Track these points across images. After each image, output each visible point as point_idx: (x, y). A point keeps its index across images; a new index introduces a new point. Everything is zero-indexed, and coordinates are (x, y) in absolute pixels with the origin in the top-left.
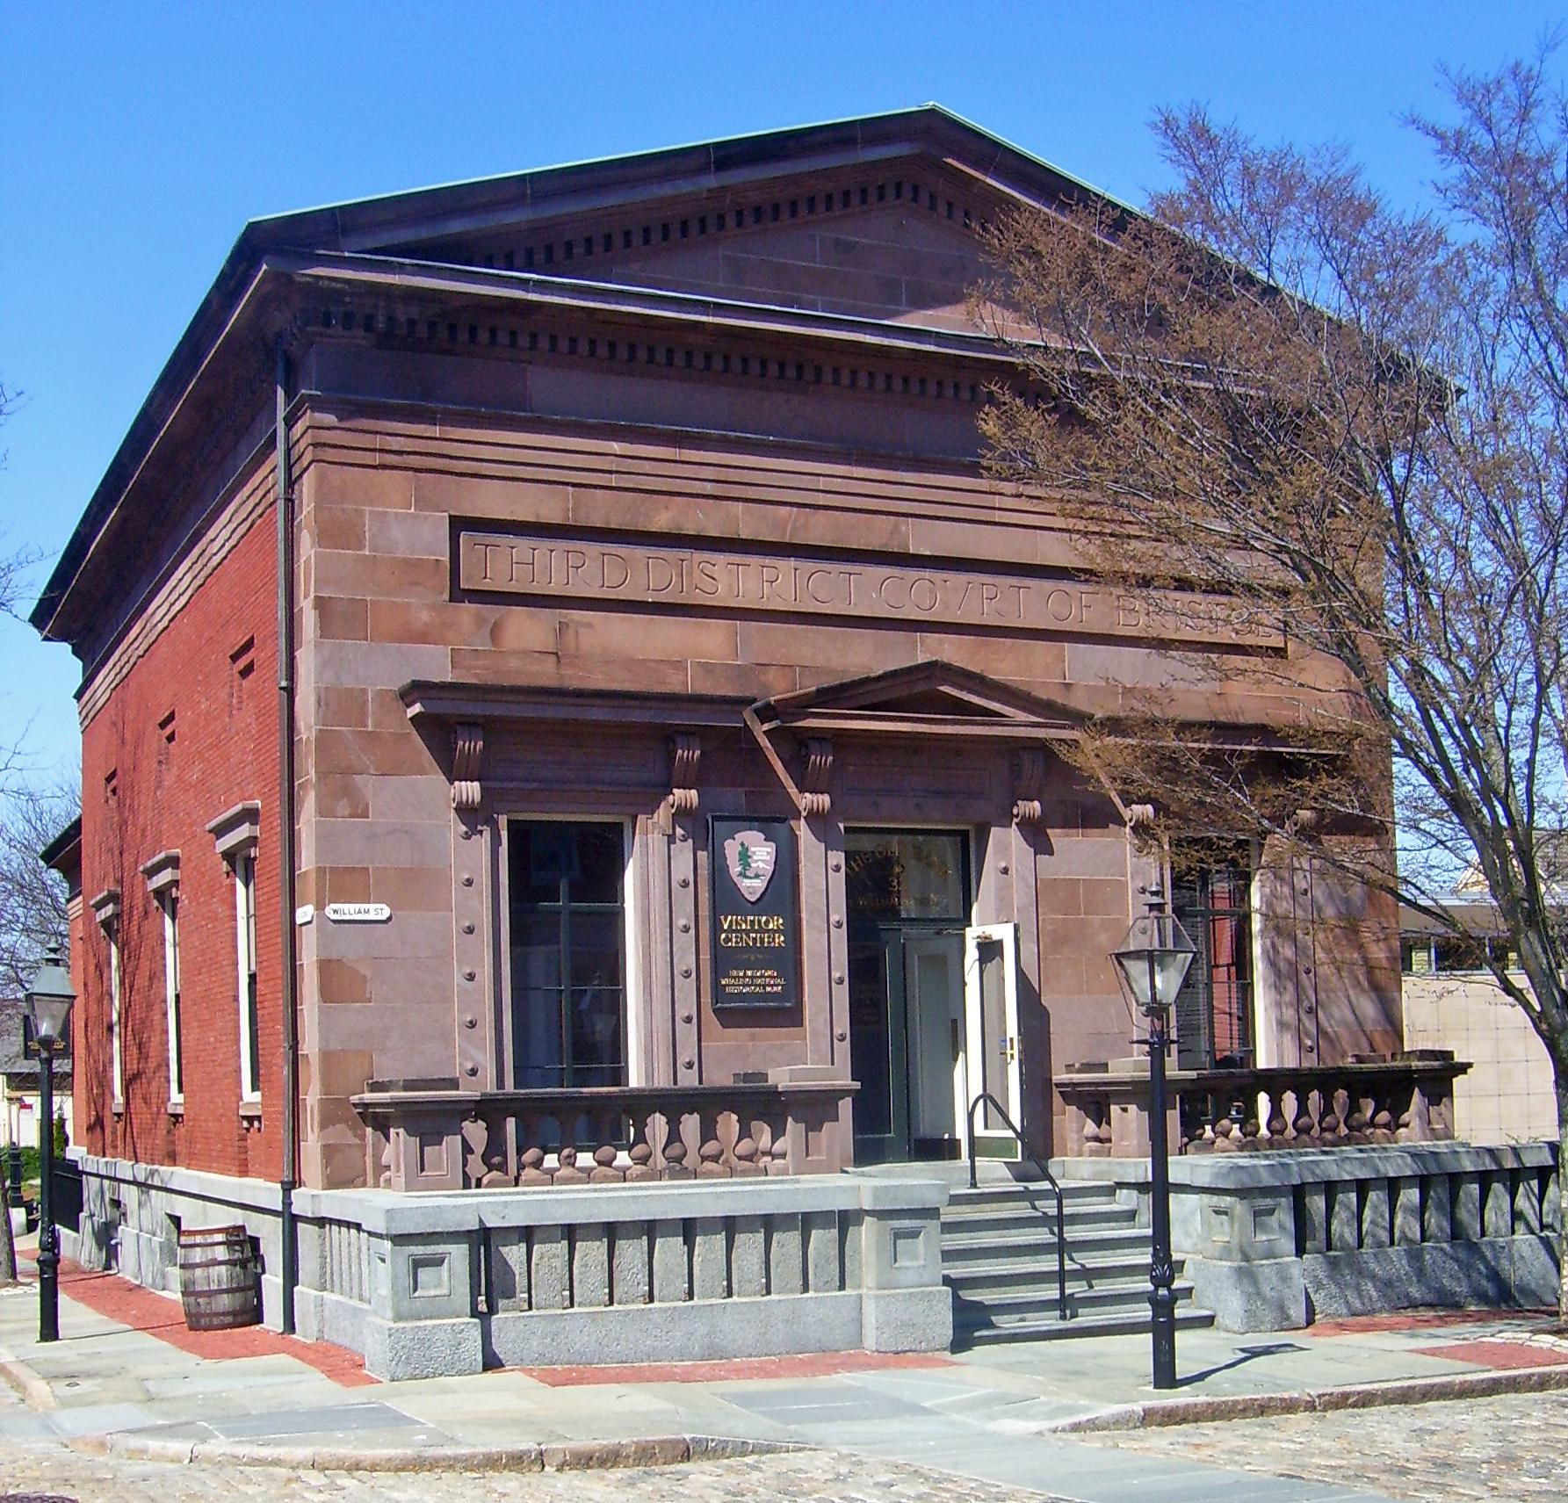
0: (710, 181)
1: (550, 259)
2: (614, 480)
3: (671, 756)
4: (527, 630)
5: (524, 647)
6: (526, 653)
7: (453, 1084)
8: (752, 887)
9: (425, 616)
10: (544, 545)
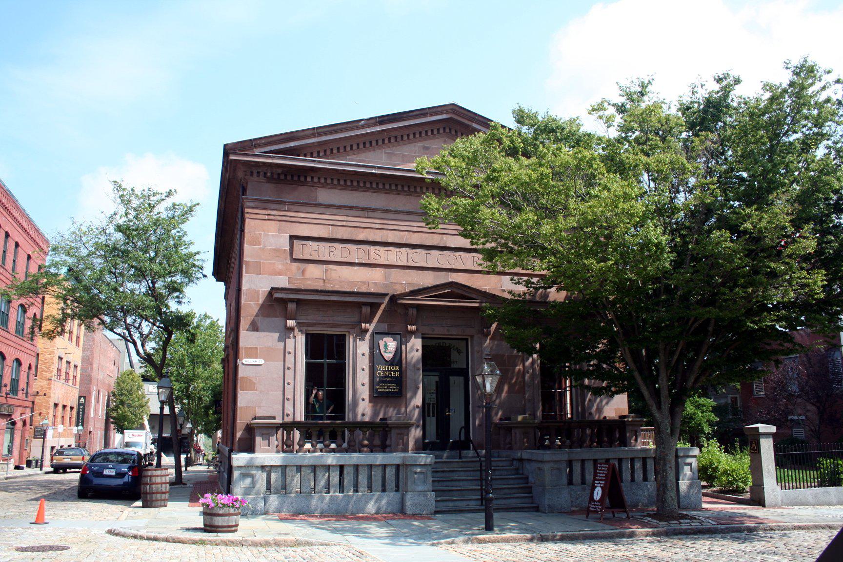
0: (378, 128)
1: (325, 154)
2: (345, 224)
3: (286, 309)
4: (314, 272)
5: (314, 277)
6: (313, 279)
7: (274, 418)
8: (388, 356)
9: (280, 267)
10: (321, 244)
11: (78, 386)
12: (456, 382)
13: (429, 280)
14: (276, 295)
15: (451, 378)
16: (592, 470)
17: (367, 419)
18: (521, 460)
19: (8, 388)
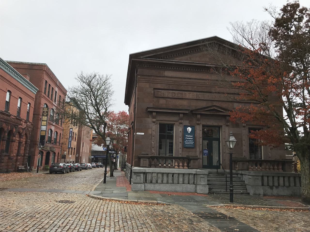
7: (148, 154)
11: (76, 141)
12: (215, 144)
13: (203, 104)
14: (149, 110)
15: (213, 142)
16: (272, 180)
17: (109, 168)
18: (242, 174)
19: (53, 141)
